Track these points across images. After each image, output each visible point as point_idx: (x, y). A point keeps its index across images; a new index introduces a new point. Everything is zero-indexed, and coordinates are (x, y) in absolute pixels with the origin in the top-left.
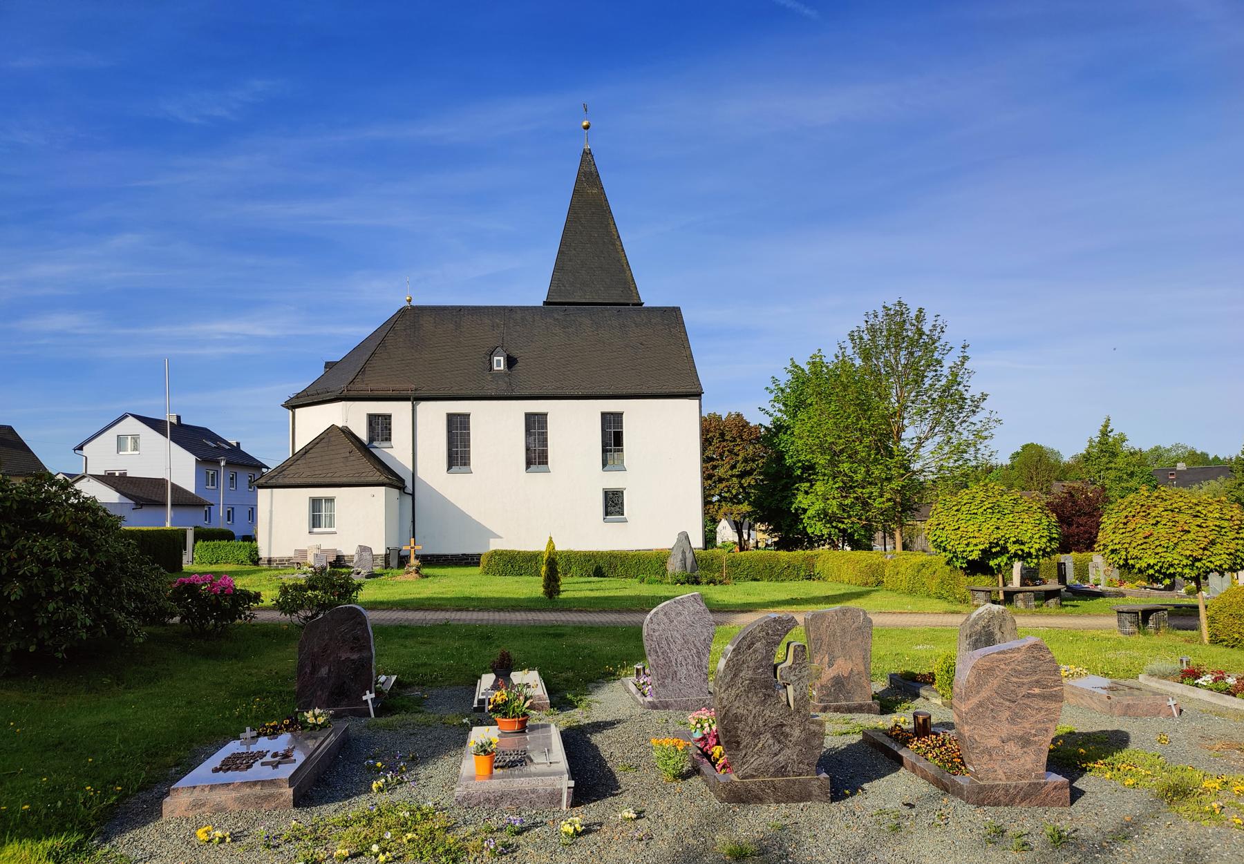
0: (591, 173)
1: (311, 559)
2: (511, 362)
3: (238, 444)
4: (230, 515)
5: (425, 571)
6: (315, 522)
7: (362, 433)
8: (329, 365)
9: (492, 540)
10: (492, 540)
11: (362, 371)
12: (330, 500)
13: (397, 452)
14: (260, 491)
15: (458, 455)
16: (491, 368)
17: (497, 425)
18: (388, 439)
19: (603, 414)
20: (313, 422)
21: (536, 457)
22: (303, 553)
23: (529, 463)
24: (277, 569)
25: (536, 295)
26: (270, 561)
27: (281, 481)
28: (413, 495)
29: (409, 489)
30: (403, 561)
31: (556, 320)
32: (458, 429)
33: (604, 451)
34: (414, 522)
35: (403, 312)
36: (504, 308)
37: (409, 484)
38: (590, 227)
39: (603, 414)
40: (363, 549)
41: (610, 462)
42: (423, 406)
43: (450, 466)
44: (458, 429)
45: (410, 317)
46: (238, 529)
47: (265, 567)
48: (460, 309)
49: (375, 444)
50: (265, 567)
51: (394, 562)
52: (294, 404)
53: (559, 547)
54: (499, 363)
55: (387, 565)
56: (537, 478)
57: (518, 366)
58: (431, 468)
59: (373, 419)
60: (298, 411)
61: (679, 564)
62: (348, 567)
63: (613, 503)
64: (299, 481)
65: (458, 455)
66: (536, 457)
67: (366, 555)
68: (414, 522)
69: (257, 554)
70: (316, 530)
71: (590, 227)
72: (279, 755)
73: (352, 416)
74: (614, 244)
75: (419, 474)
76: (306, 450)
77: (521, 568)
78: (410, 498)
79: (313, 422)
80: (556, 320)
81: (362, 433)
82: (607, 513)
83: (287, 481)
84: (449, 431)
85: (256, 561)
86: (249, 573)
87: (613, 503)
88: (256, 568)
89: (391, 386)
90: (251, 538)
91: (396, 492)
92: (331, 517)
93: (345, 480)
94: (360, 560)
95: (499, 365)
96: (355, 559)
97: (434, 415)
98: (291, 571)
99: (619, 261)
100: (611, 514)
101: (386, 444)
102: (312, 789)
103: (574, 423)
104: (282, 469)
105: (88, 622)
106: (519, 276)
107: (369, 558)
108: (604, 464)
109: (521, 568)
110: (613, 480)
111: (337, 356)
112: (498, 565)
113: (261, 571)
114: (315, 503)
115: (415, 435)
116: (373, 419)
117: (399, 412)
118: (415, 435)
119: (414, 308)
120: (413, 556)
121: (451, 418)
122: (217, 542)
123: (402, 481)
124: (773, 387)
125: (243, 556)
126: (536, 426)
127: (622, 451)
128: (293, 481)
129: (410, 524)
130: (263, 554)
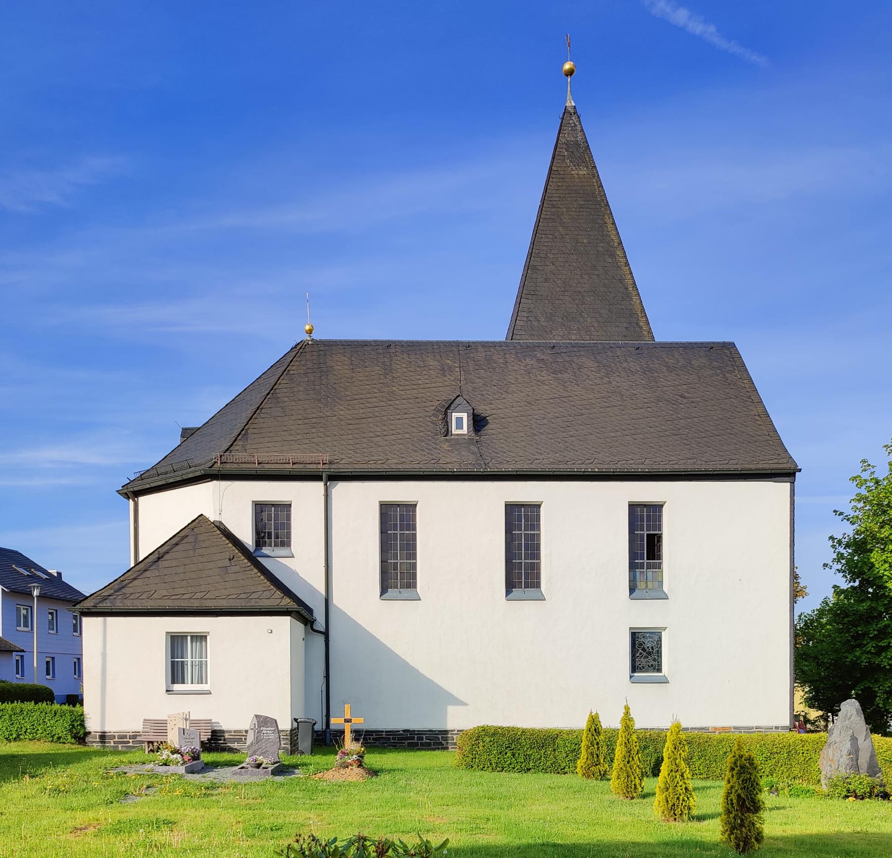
0: (577, 144)
1: (173, 738)
2: (478, 422)
3: (59, 574)
4: (49, 667)
5: (373, 759)
6: (176, 673)
7: (246, 535)
8: (188, 433)
9: (451, 709)
10: (451, 709)
11: (243, 434)
12: (200, 638)
14: (86, 621)
16: (447, 432)
17: (460, 520)
18: (285, 542)
19: (633, 507)
20: (164, 516)
21: (522, 570)
22: (160, 726)
23: (510, 585)
24: (115, 752)
25: (499, 334)
26: (103, 737)
27: (119, 605)
28: (326, 634)
29: (320, 624)
30: (326, 740)
31: (539, 360)
32: (397, 525)
33: (633, 566)
34: (327, 677)
35: (300, 349)
36: (458, 344)
38: (575, 226)
39: (633, 507)
40: (263, 721)
41: (641, 585)
42: (341, 489)
43: (384, 590)
44: (397, 525)
45: (310, 359)
46: (59, 688)
47: (96, 746)
48: (388, 345)
49: (266, 550)
50: (96, 746)
51: (305, 743)
52: (135, 491)
53: (639, 723)
54: (460, 423)
55: (294, 749)
56: (525, 609)
57: (491, 428)
58: (356, 593)
60: (142, 500)
61: (845, 760)
62: (231, 750)
63: (645, 652)
64: (150, 605)
66: (522, 570)
67: (267, 731)
68: (327, 677)
69: (82, 725)
70: (177, 687)
71: (575, 226)
73: (230, 505)
74: (613, 255)
75: (337, 600)
76: (159, 555)
77: (527, 757)
78: (321, 639)
79: (164, 516)
80: (539, 360)
81: (246, 535)
82: (634, 669)
83: (129, 605)
84: (383, 532)
85: (81, 737)
86: (68, 759)
87: (645, 652)
88: (81, 749)
89: (291, 456)
90: (75, 700)
91: (300, 626)
92: (202, 666)
93: (224, 604)
94: (258, 740)
95: (459, 425)
96: (250, 738)
97: (359, 505)
98: (137, 756)
99: (621, 280)
100: (642, 669)
103: (584, 521)
104: (119, 585)
106: (470, 297)
107: (273, 736)
108: (632, 590)
109: (527, 757)
110: (645, 615)
111: (197, 422)
112: (490, 752)
113: (88, 755)
114: (176, 641)
116: (260, 508)
117: (305, 498)
118: (331, 533)
119: (316, 343)
120: (348, 736)
121: (387, 510)
122: (17, 705)
123: (310, 611)
124: (866, 476)
125: (61, 728)
126: (522, 524)
127: (659, 566)
128: (139, 605)
129: (321, 680)
130: (93, 725)
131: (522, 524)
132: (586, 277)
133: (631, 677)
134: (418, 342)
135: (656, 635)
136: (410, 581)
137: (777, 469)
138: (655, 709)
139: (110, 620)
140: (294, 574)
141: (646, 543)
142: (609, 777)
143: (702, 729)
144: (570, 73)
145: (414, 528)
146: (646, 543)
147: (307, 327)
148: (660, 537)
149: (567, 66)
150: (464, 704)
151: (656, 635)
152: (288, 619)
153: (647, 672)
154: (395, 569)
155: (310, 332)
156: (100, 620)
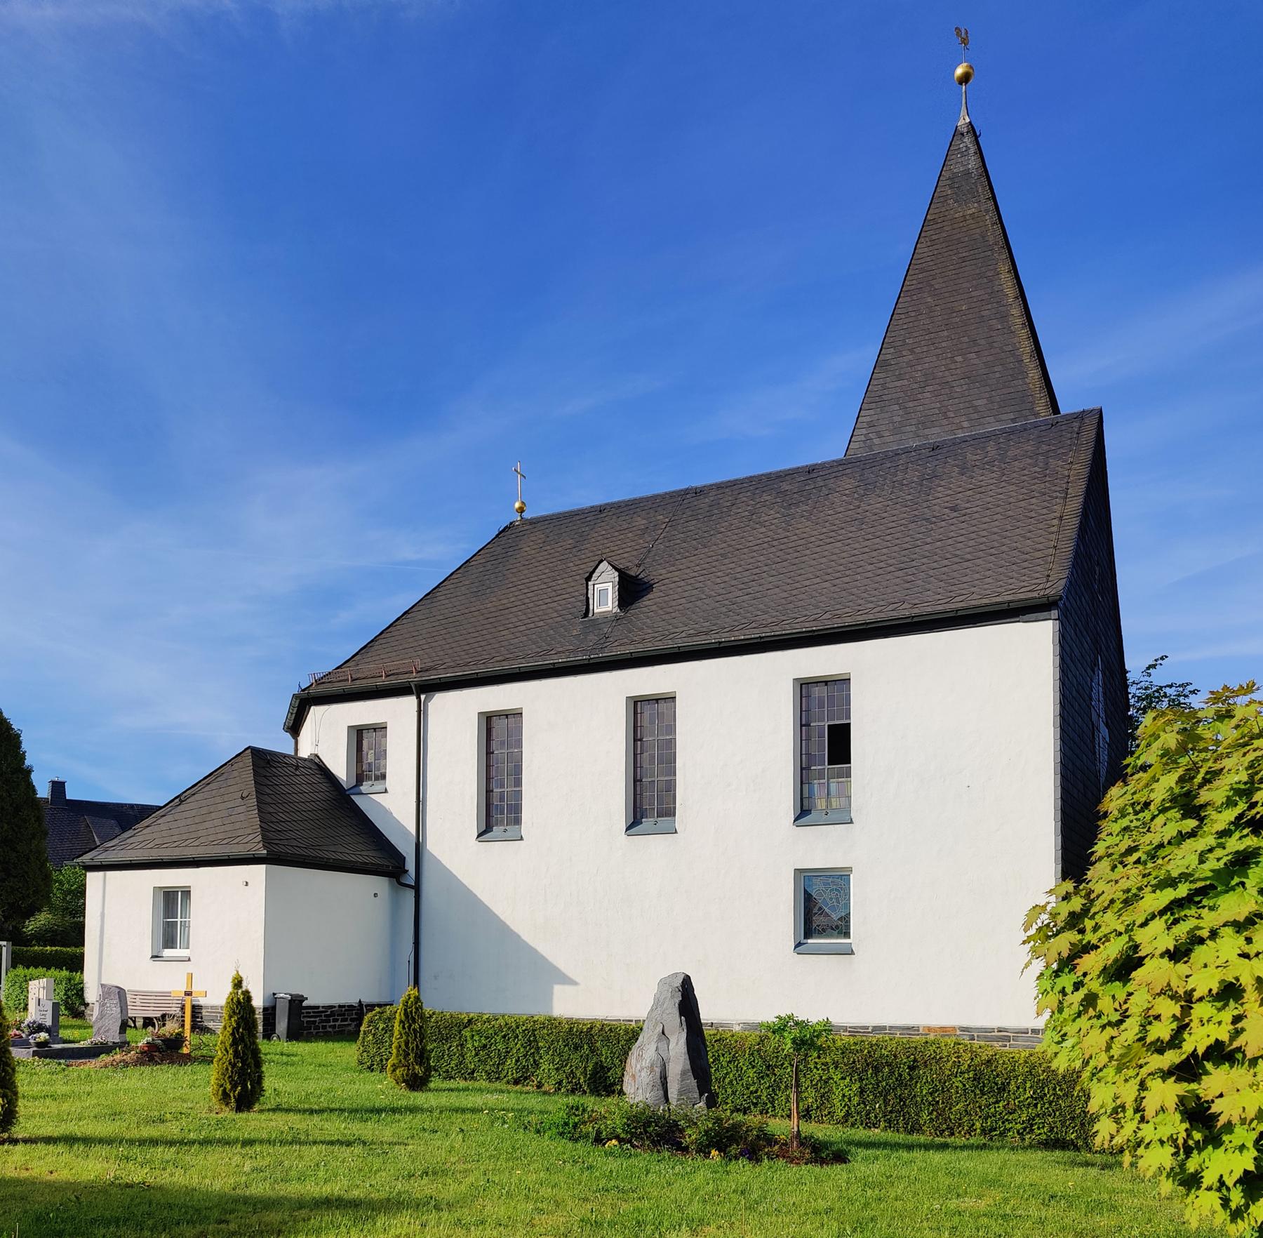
9: (558, 989)
10: (558, 989)
13: (392, 804)
15: (499, 810)
17: (574, 725)
21: (650, 799)
23: (635, 821)
28: (417, 888)
32: (499, 740)
37: (410, 865)
42: (442, 703)
44: (499, 740)
56: (652, 847)
59: (358, 734)
63: (821, 912)
65: (499, 810)
66: (650, 799)
70: (168, 953)
72: (1214, 992)
75: (433, 845)
87: (821, 912)
91: (379, 884)
97: (455, 713)
100: (822, 932)
101: (378, 786)
102: (1193, 990)
103: (735, 712)
105: (815, 1054)
108: (803, 812)
110: (821, 848)
115: (424, 760)
116: (358, 734)
117: (396, 714)
123: (401, 859)
126: (649, 727)
131: (649, 727)
132: (959, 359)
133: (798, 945)
134: (641, 499)
135: (838, 880)
136: (515, 815)
137: (992, 605)
138: (855, 995)
139: (109, 873)
140: (387, 813)
141: (827, 742)
142: (1222, 1120)
143: (908, 1028)
144: (965, 79)
145: (519, 744)
146: (827, 742)
147: (517, 505)
148: (846, 728)
149: (959, 71)
150: (574, 983)
151: (838, 880)
152: (262, 868)
153: (831, 936)
154: (502, 799)
155: (521, 510)
156: (101, 873)
